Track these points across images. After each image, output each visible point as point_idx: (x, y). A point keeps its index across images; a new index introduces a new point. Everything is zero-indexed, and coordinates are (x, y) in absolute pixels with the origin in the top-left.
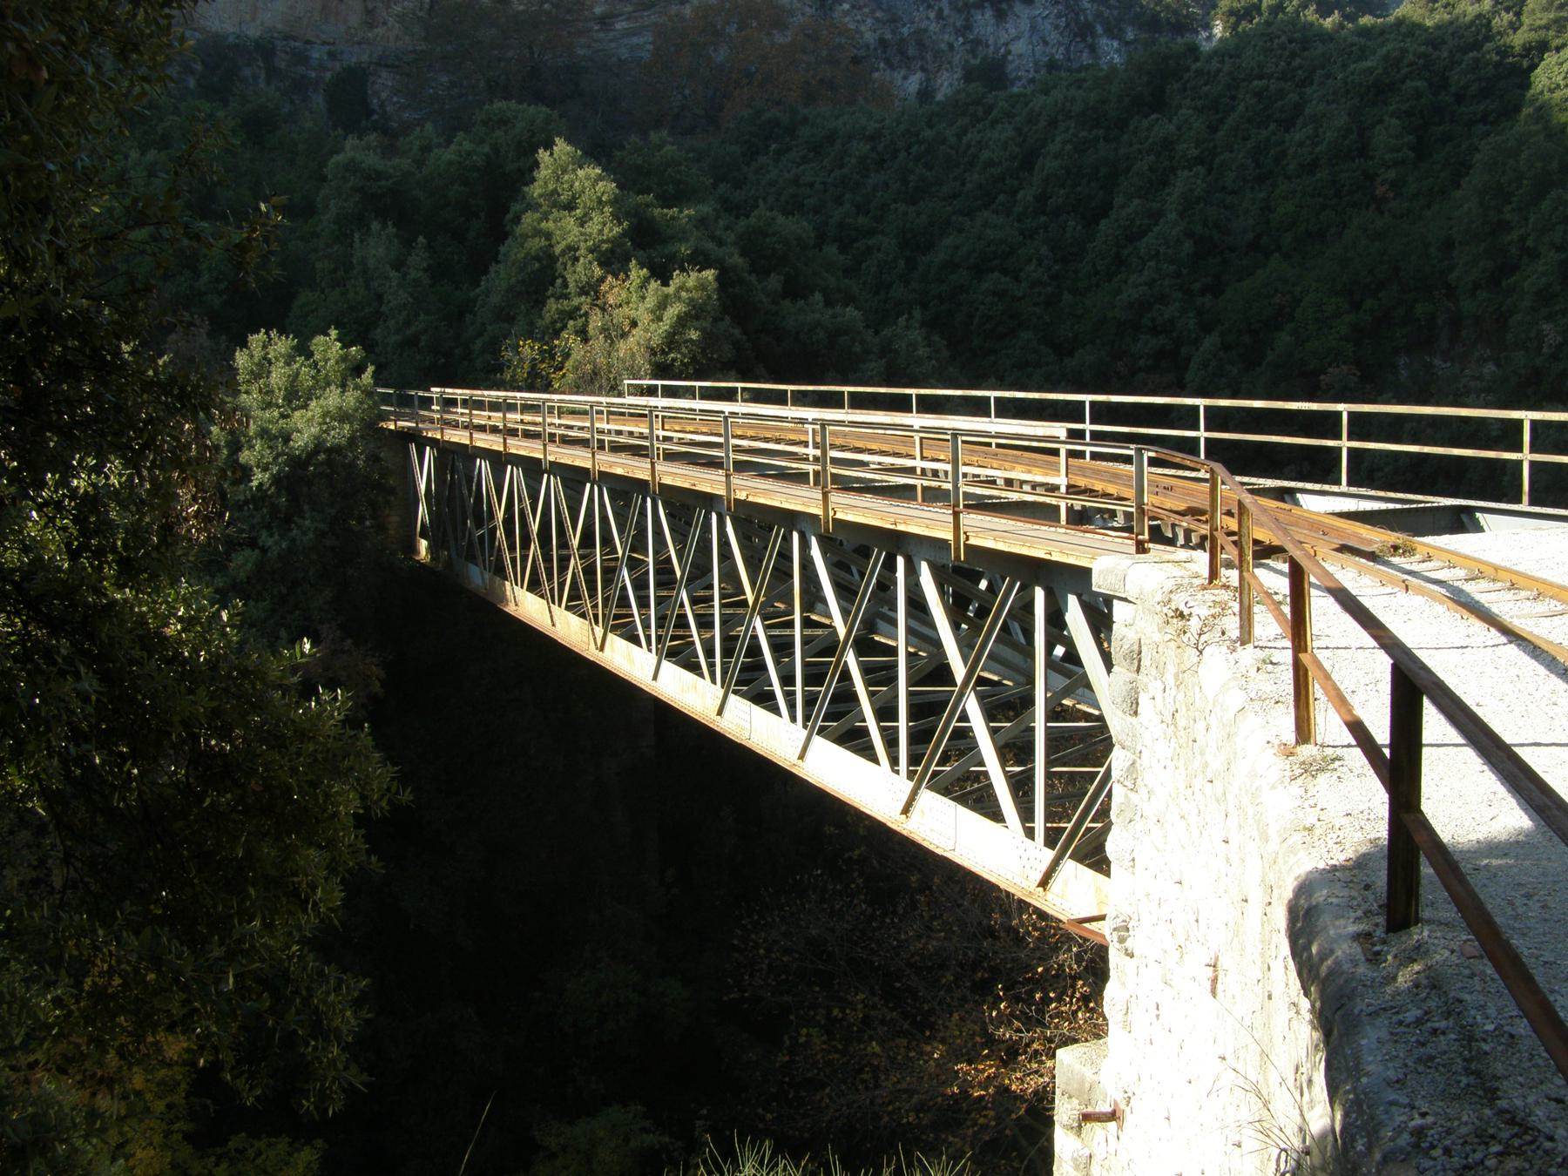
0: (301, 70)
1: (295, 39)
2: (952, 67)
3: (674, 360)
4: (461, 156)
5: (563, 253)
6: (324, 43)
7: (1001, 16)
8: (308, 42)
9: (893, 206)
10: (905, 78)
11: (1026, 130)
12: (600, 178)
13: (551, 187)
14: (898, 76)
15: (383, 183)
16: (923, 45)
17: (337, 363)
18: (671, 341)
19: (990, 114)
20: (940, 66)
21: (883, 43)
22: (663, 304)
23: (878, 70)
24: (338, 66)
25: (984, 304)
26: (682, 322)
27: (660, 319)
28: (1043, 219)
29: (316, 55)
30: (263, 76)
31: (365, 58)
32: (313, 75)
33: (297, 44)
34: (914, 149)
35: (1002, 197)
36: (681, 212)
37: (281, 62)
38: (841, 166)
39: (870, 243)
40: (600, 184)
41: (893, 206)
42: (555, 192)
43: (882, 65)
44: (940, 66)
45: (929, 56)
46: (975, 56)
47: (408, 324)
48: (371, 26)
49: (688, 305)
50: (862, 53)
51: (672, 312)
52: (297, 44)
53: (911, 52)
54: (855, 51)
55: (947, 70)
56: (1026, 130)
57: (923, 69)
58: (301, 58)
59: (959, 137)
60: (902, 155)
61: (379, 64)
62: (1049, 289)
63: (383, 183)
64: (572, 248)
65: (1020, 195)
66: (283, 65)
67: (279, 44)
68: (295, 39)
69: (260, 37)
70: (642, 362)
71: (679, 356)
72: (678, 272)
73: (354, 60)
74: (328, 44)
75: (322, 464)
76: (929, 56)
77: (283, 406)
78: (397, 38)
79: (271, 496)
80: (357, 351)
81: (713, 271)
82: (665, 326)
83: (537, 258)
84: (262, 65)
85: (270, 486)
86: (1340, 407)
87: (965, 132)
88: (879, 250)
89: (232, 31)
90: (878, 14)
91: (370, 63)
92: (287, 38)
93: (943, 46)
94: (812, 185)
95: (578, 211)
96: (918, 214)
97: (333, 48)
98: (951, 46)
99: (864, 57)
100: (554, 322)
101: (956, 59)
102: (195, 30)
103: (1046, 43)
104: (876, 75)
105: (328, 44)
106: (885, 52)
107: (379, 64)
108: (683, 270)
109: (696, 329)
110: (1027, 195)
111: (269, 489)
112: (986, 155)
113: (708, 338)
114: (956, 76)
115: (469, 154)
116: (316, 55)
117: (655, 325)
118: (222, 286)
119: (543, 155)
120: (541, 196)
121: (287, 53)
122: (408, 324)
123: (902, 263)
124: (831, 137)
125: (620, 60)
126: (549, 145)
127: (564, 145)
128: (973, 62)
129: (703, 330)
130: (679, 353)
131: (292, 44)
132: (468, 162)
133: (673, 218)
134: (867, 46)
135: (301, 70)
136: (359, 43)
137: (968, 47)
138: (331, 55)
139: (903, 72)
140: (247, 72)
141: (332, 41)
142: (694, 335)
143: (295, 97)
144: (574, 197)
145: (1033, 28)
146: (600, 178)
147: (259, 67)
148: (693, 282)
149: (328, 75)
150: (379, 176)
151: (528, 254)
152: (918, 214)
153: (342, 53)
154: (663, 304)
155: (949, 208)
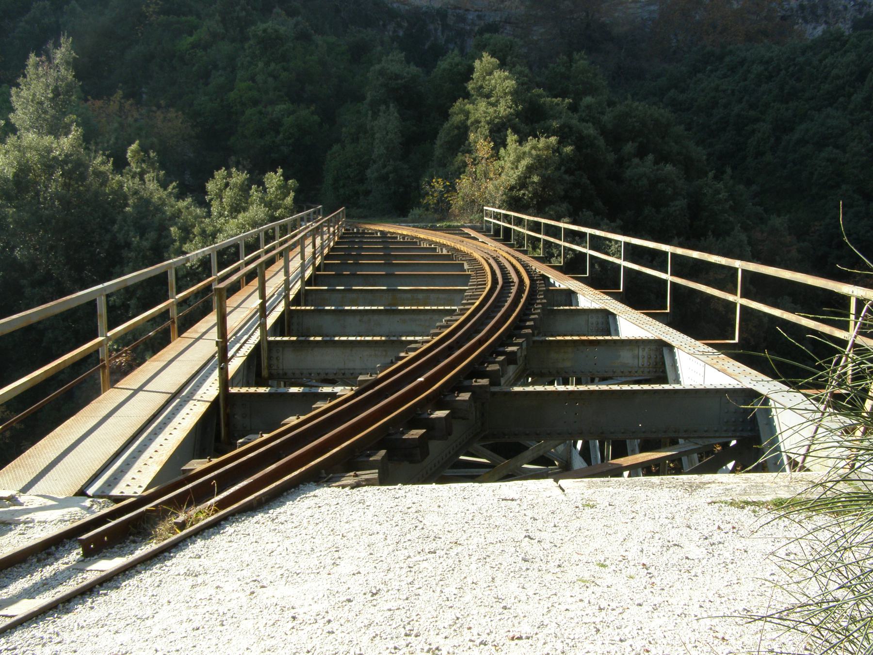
0: (462, 25)
1: (460, 8)
2: (845, 21)
3: (524, 194)
4: (452, 66)
5: (472, 123)
6: (476, 11)
8: (467, 10)
9: (772, 104)
10: (815, 28)
11: (864, 56)
12: (507, 78)
13: (479, 83)
14: (809, 28)
15: (399, 81)
16: (828, 8)
17: (277, 189)
18: (522, 183)
19: (844, 46)
20: (837, 20)
22: (519, 159)
23: (798, 23)
24: (482, 23)
25: (820, 167)
26: (530, 169)
27: (517, 168)
28: (867, 113)
29: (470, 17)
30: (440, 29)
31: (498, 19)
32: (468, 28)
33: (460, 11)
34: (791, 69)
35: (841, 99)
36: (563, 100)
37: (451, 20)
38: (745, 80)
39: (755, 127)
40: (506, 82)
41: (772, 104)
42: (481, 87)
43: (800, 21)
44: (837, 20)
45: (830, 14)
46: (861, 13)
47: (384, 166)
49: (535, 159)
50: (789, 13)
51: (524, 163)
52: (460, 11)
53: (820, 12)
54: (784, 12)
55: (842, 22)
56: (864, 56)
57: (826, 23)
58: (462, 19)
59: (821, 61)
60: (783, 72)
61: (506, 22)
62: (865, 158)
63: (399, 81)
64: (477, 122)
65: (853, 98)
66: (451, 23)
67: (450, 12)
68: (460, 8)
69: (441, 8)
70: (499, 196)
71: (527, 192)
72: (531, 138)
73: (491, 20)
74: (478, 11)
75: (233, 254)
76: (830, 14)
77: (228, 216)
78: (517, 8)
79: (198, 273)
80: (292, 183)
81: (555, 137)
82: (518, 173)
83: (458, 128)
84: (440, 22)
85: (199, 266)
86: (737, 264)
87: (825, 57)
88: (759, 132)
89: (425, 4)
91: (500, 21)
92: (456, 8)
93: (840, 8)
94: (724, 91)
95: (492, 99)
96: (787, 109)
97: (480, 13)
98: (845, 8)
99: (790, 16)
100: (459, 168)
101: (848, 16)
102: (405, 4)
104: (796, 27)
105: (478, 11)
106: (803, 13)
107: (506, 22)
108: (535, 136)
109: (538, 175)
110: (858, 97)
111: (197, 268)
112: (835, 72)
113: (546, 182)
114: (847, 26)
115: (457, 65)
116: (470, 17)
117: (513, 171)
118: (290, 141)
119: (477, 63)
120: (473, 89)
121: (454, 16)
122: (384, 166)
123: (772, 140)
124: (742, 63)
125: (642, 19)
126: (480, 58)
127: (489, 58)
128: (859, 17)
129: (542, 176)
130: (528, 190)
131: (458, 11)
132: (455, 70)
133: (558, 104)
134: (792, 9)
135: (462, 25)
136: (496, 10)
137: (857, 7)
138: (479, 17)
139: (813, 25)
140: (431, 27)
141: (480, 9)
142: (536, 179)
143: (457, 40)
144: (492, 90)
146: (507, 78)
147: (438, 24)
148: (545, 142)
149: (476, 28)
150: (397, 77)
151: (453, 124)
152: (787, 109)
153: (485, 16)
154: (519, 159)
155: (807, 106)
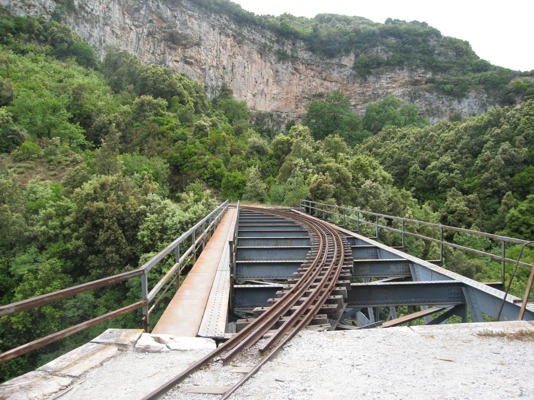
7: (459, 102)
21: (427, 110)
48: (297, 108)
90: (426, 103)
103: (472, 109)
134: (423, 111)
145: (469, 105)
